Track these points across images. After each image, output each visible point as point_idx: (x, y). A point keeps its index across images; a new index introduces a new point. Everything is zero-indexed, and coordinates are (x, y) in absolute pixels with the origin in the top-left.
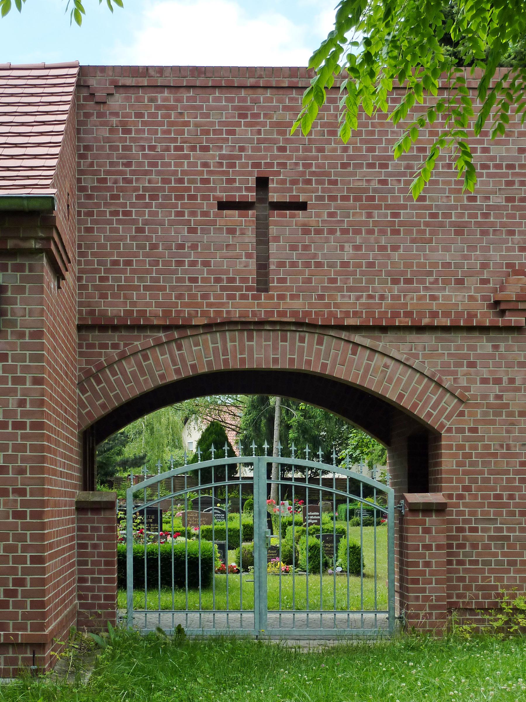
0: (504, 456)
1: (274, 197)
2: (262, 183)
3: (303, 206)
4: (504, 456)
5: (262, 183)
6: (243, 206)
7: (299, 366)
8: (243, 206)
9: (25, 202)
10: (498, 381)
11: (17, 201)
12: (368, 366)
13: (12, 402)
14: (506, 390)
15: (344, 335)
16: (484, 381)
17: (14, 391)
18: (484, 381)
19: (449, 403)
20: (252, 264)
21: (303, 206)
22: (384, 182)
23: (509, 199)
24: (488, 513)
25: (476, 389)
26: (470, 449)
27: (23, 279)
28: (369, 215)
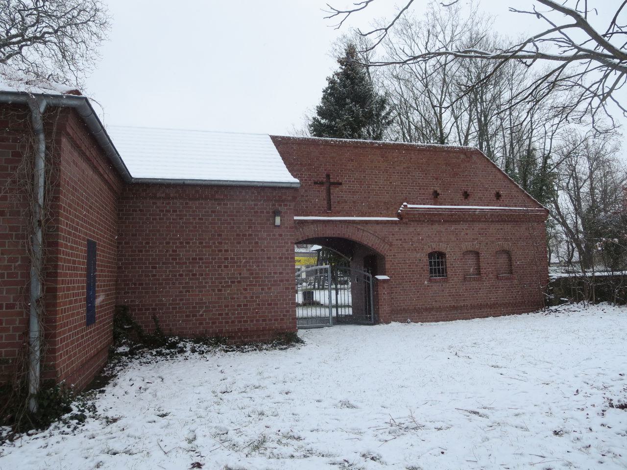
0: (403, 263)
1: (332, 180)
2: (328, 176)
3: (341, 184)
4: (403, 263)
5: (328, 176)
6: (322, 183)
7: (341, 236)
8: (322, 183)
9: (202, 182)
10: (401, 240)
11: (152, 180)
12: (362, 235)
13: (284, 250)
14: (403, 242)
15: (355, 225)
16: (397, 240)
17: (285, 246)
18: (397, 240)
19: (387, 247)
20: (325, 202)
21: (341, 184)
22: (365, 177)
23: (401, 183)
24: (253, 281)
25: (395, 242)
26: (186, 262)
27: (287, 209)
28: (361, 187)
